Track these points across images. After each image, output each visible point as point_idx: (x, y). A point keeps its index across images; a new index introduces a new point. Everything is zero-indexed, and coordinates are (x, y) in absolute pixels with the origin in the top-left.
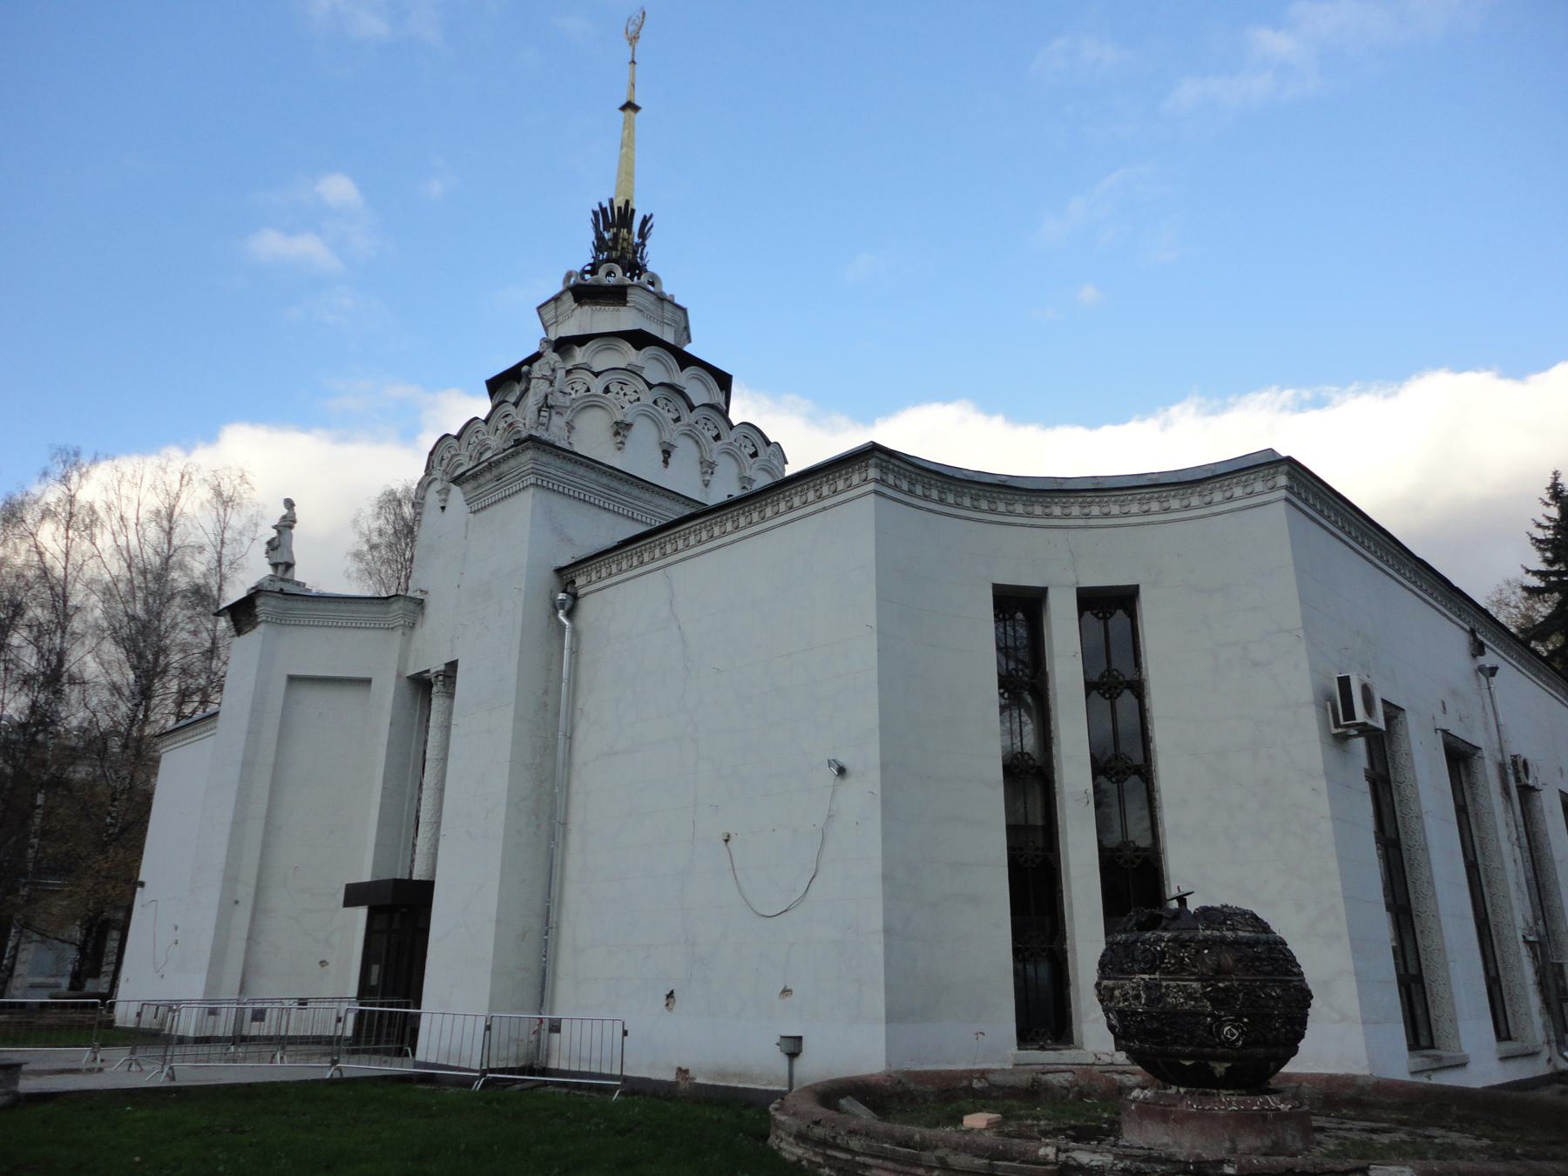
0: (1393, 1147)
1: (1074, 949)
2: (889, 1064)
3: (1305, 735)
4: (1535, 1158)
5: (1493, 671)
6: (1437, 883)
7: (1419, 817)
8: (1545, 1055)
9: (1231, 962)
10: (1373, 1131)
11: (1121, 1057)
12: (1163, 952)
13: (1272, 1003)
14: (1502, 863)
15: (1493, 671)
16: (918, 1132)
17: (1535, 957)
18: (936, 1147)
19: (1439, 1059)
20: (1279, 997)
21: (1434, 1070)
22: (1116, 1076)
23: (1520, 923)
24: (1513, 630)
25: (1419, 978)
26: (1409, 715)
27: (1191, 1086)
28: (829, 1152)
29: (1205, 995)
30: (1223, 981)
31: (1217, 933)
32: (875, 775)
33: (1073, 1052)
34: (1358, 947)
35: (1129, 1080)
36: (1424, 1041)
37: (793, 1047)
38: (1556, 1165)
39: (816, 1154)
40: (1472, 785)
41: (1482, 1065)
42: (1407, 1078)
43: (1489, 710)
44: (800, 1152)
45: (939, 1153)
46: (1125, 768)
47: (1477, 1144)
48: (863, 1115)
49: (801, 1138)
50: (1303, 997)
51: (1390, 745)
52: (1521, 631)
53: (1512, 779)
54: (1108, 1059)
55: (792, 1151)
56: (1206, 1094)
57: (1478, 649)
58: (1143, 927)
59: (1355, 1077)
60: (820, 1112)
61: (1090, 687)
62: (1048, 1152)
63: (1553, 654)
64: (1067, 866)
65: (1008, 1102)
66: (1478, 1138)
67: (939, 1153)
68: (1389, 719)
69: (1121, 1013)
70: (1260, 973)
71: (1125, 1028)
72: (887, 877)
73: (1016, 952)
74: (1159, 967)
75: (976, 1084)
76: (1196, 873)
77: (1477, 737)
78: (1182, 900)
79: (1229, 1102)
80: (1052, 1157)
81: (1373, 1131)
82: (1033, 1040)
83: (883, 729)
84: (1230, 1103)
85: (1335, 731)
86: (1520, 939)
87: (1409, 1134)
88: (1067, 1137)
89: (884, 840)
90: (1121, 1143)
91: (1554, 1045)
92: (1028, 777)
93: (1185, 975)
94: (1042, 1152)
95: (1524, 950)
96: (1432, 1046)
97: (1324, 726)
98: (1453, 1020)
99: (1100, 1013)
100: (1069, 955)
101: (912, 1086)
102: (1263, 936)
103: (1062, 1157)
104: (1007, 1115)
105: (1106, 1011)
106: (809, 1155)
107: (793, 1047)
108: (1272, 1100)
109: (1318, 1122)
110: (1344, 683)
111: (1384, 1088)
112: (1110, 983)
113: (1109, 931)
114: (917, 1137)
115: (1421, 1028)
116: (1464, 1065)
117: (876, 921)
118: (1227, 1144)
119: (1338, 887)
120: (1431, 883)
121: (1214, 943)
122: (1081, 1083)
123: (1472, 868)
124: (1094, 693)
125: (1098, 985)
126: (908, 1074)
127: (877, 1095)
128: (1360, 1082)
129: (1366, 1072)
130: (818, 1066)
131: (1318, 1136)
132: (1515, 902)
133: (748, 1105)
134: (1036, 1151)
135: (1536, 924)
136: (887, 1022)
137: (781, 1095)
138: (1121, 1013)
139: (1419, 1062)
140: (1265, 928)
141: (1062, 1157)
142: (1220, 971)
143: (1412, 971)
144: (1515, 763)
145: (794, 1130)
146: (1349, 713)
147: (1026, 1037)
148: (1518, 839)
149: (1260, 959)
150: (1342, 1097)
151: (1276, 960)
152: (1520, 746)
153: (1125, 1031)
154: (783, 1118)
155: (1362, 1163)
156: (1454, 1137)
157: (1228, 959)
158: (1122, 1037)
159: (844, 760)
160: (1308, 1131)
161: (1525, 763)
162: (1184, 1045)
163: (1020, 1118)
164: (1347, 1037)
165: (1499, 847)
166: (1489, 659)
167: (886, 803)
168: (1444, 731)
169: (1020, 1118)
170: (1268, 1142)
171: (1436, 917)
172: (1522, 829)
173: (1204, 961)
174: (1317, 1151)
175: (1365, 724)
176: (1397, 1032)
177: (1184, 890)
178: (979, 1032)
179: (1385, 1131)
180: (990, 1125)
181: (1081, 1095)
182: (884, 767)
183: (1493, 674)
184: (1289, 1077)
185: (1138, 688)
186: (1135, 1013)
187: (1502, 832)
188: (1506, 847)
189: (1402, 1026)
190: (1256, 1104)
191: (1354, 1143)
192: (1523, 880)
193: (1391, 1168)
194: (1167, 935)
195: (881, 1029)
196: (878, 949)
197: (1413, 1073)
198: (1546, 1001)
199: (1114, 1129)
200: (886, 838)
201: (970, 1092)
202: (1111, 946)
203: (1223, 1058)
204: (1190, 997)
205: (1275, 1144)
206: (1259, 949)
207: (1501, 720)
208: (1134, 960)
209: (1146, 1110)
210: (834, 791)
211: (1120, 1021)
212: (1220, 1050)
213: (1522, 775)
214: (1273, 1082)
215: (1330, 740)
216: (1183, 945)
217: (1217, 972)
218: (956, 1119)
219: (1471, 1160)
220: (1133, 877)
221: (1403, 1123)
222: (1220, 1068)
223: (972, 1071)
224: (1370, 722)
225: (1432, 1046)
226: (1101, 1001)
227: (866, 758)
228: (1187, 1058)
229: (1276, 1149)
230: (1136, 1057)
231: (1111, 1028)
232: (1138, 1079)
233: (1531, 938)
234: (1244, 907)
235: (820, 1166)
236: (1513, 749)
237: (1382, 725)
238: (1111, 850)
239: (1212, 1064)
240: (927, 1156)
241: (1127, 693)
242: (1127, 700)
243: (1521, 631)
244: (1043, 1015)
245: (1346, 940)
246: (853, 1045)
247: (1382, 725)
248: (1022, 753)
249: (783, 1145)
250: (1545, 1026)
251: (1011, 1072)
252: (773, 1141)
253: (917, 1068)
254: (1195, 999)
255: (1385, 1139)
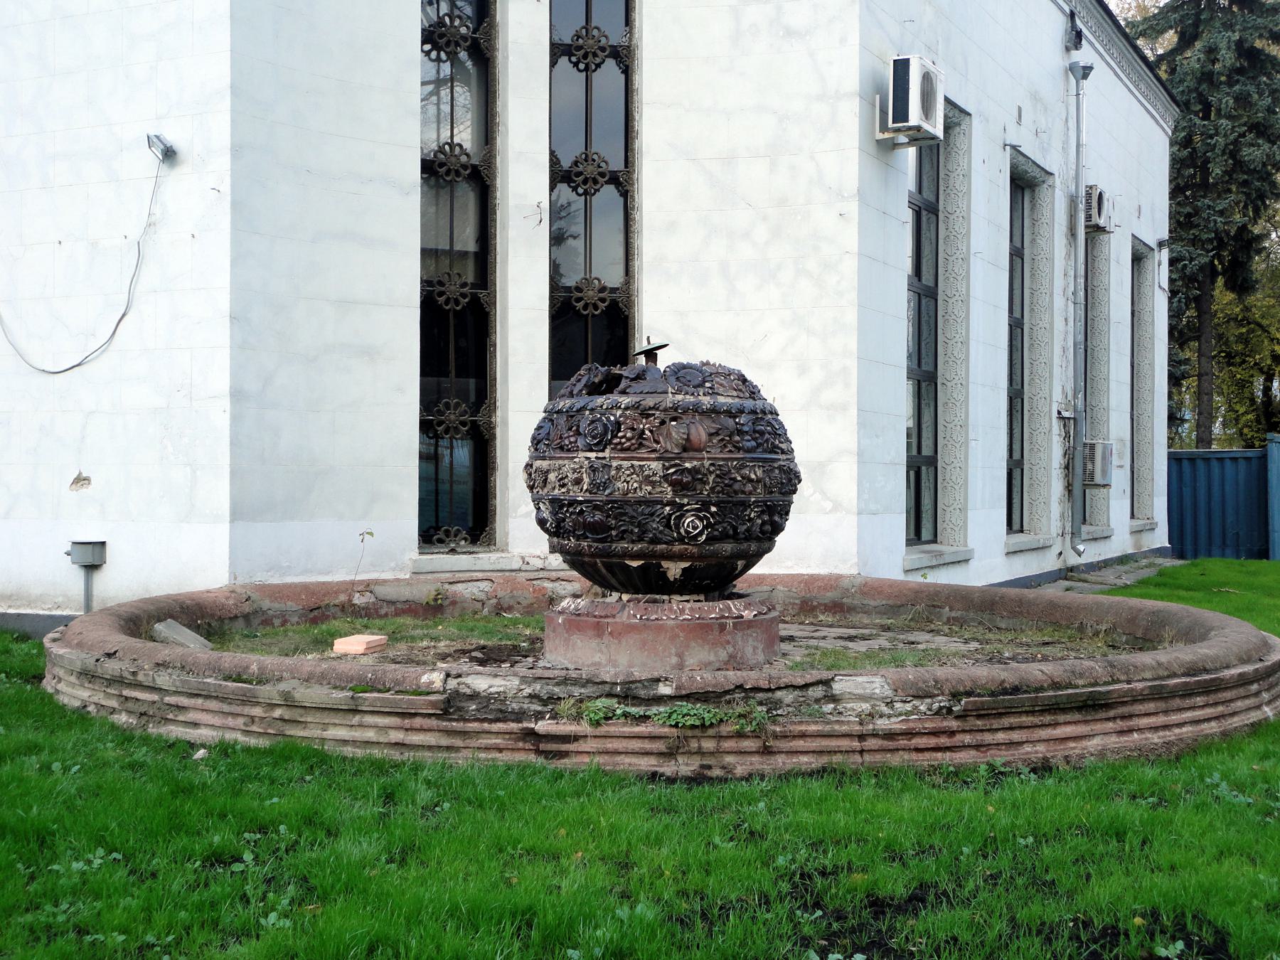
0: (869, 655)
1: (505, 423)
3: (848, 125)
5: (1086, 71)
7: (966, 260)
8: (1056, 550)
9: (704, 437)
10: (851, 638)
11: (556, 561)
12: (618, 424)
13: (749, 487)
15: (1086, 71)
16: (255, 661)
18: (280, 679)
19: (941, 554)
20: (759, 481)
21: (932, 567)
22: (547, 585)
23: (1057, 396)
24: (1123, 23)
25: (933, 461)
28: (126, 692)
29: (665, 477)
31: (690, 399)
32: (223, 163)
33: (494, 556)
36: (926, 534)
37: (91, 557)
39: (108, 695)
40: (1034, 222)
41: (985, 556)
42: (898, 575)
44: (85, 694)
45: (283, 686)
46: (596, 176)
47: (963, 647)
48: (191, 644)
49: (88, 676)
52: (1128, 23)
53: (1082, 217)
54: (538, 564)
55: (72, 693)
56: (655, 601)
57: (1076, 39)
58: (594, 390)
59: (839, 577)
60: (119, 641)
61: (558, 51)
62: (434, 678)
63: (1160, 58)
64: (505, 309)
65: (400, 620)
67: (283, 686)
68: (947, 128)
69: (556, 503)
70: (739, 449)
71: (559, 522)
74: (610, 442)
75: (358, 600)
76: (675, 321)
78: (651, 354)
79: (681, 608)
80: (438, 685)
81: (851, 638)
82: (440, 541)
83: (236, 90)
84: (682, 611)
85: (880, 136)
86: (1055, 414)
87: (890, 640)
88: (472, 659)
90: (541, 663)
91: (1068, 537)
92: (459, 178)
93: (643, 453)
95: (1056, 427)
96: (934, 541)
97: (866, 131)
98: (964, 510)
99: (531, 507)
100: (498, 431)
101: (266, 604)
102: (749, 404)
103: (452, 684)
104: (394, 637)
105: (537, 501)
106: (99, 698)
107: (91, 557)
108: (735, 606)
109: (785, 630)
110: (901, 67)
111: (871, 588)
112: (544, 464)
113: (552, 395)
114: (254, 667)
115: (923, 521)
116: (967, 561)
117: (218, 378)
118: (674, 660)
119: (853, 345)
121: (685, 411)
122: (500, 594)
123: (1016, 326)
124: (563, 61)
125: (529, 466)
127: (207, 618)
129: (854, 571)
130: (124, 581)
131: (785, 647)
132: (1057, 371)
133: (24, 638)
135: (1075, 397)
136: (232, 521)
137: (66, 621)
138: (556, 503)
139: (919, 556)
140: (754, 393)
141: (452, 684)
142: (688, 447)
143: (927, 451)
144: (1089, 195)
145: (78, 666)
146: (901, 112)
149: (740, 432)
150: (826, 602)
151: (762, 433)
152: (1096, 176)
153: (560, 523)
154: (61, 651)
155: (826, 675)
156: (940, 640)
157: (700, 432)
159: (173, 137)
160: (774, 640)
162: (633, 542)
163: (413, 639)
164: (833, 531)
166: (1084, 55)
169: (413, 639)
170: (723, 655)
175: (918, 128)
176: (898, 524)
177: (655, 342)
178: (371, 531)
179: (864, 638)
180: (370, 649)
181: (499, 609)
182: (237, 151)
183: (1085, 76)
184: (761, 579)
185: (624, 58)
187: (1059, 282)
194: (625, 401)
195: (223, 531)
196: (220, 416)
197: (907, 571)
198: (1069, 488)
199: (535, 647)
200: (237, 260)
201: (349, 610)
203: (680, 557)
204: (647, 480)
208: (578, 433)
209: (576, 622)
210: (157, 185)
211: (554, 513)
212: (677, 548)
213: (1094, 211)
214: (740, 585)
215: (872, 148)
216: (645, 414)
217: (685, 449)
218: (324, 643)
219: (954, 665)
220: (594, 330)
222: (674, 570)
223: (353, 583)
224: (926, 126)
226: (531, 488)
227: (208, 135)
228: (635, 556)
230: (575, 560)
231: (541, 523)
235: (113, 711)
236: (1089, 178)
237: (939, 131)
239: (665, 564)
241: (610, 64)
242: (609, 72)
243: (1128, 23)
244: (456, 509)
245: (854, 412)
246: (182, 548)
247: (939, 131)
249: (61, 686)
250: (1062, 516)
251: (408, 582)
252: (48, 685)
254: (653, 484)
255: (861, 646)
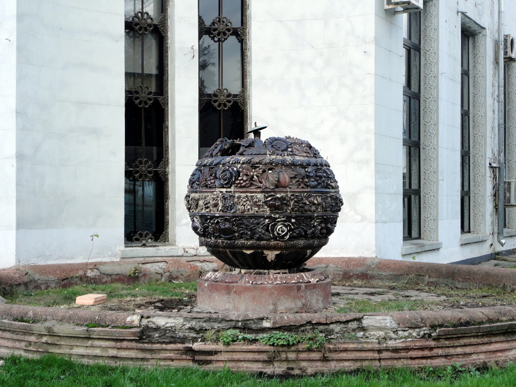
0: (383, 304)
1: (174, 172)
6: (441, 126)
8: (489, 243)
9: (288, 179)
10: (372, 294)
11: (204, 250)
12: (238, 172)
13: (313, 208)
14: (485, 113)
17: (495, 177)
18: (45, 320)
20: (319, 204)
22: (198, 264)
25: (418, 192)
29: (266, 203)
31: (279, 158)
33: (168, 248)
36: (414, 234)
38: (483, 310)
41: (449, 246)
45: (47, 324)
47: (437, 299)
50: (337, 204)
51: (425, 20)
53: (502, 53)
54: (193, 252)
56: (260, 273)
58: (225, 153)
59: (365, 259)
64: (173, 107)
65: (114, 285)
66: (438, 296)
67: (47, 324)
70: (308, 186)
71: (205, 229)
72: (20, 113)
75: (90, 274)
76: (274, 112)
77: (484, 20)
78: (257, 133)
79: (275, 278)
80: (136, 323)
81: (372, 294)
82: (137, 240)
84: (276, 279)
85: (387, 7)
87: (395, 295)
88: (156, 307)
90: (195, 310)
93: (253, 188)
94: (129, 319)
95: (489, 172)
96: (419, 238)
98: (436, 220)
100: (170, 177)
101: (37, 277)
102: (313, 160)
104: (111, 295)
105: (192, 217)
108: (306, 276)
109: (334, 289)
112: (196, 195)
113: (201, 156)
114: (31, 313)
115: (413, 225)
118: (271, 307)
119: (372, 125)
120: (436, 125)
122: (171, 269)
123: (465, 115)
125: (187, 196)
126: (35, 268)
128: (369, 262)
129: (374, 255)
131: (335, 299)
132: (489, 140)
135: (499, 155)
140: (316, 154)
141: (145, 322)
143: (414, 187)
144: (506, 40)
147: (131, 236)
149: (308, 177)
150: (358, 273)
151: (321, 177)
155: (358, 315)
157: (285, 176)
161: (512, 41)
163: (122, 296)
164: (364, 233)
165: (485, 101)
167: (19, 49)
168: (463, 13)
169: (122, 296)
170: (299, 304)
171: (436, 149)
177: (259, 125)
179: (380, 294)
180: (97, 302)
181: (171, 278)
182: (20, 17)
184: (321, 260)
186: (213, 217)
188: (489, 101)
189: (402, 224)
190: (294, 278)
192: (496, 124)
193: (378, 318)
194: (242, 159)
197: (403, 255)
200: (20, 78)
202: (200, 167)
203: (274, 248)
204: (256, 204)
205: (304, 305)
206: (309, 169)
207: (503, 8)
208: (215, 178)
209: (215, 286)
211: (202, 223)
212: (273, 243)
213: (509, 50)
214: (309, 264)
215: (383, 14)
216: (254, 166)
218: (70, 299)
220: (224, 119)
221: (393, 288)
222: (271, 255)
223: (87, 264)
226: (189, 209)
228: (248, 248)
229: (454, 343)
230: (214, 250)
231: (195, 229)
232: (211, 266)
233: (494, 165)
234: (303, 139)
236: (506, 31)
238: (209, 95)
239: (266, 252)
240: (38, 327)
244: (146, 221)
245: (372, 165)
248: (142, 13)
250: (492, 223)
251: (118, 263)
254: (259, 206)
255: (378, 299)
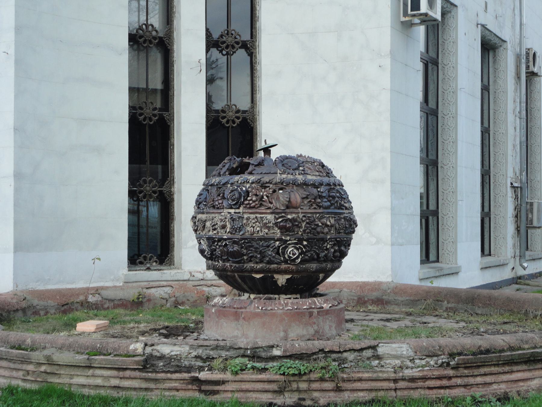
0: (399, 331)
1: (180, 191)
2: (16, 285)
4: (493, 333)
8: (510, 266)
9: (299, 200)
10: (388, 320)
11: (211, 274)
12: (247, 192)
13: (326, 230)
14: (507, 130)
17: (516, 198)
18: (45, 348)
19: (441, 269)
20: (332, 226)
21: (436, 277)
22: (206, 289)
26: (460, 10)
27: (259, 293)
29: (276, 224)
30: (291, 213)
31: (290, 177)
34: (396, 190)
35: (214, 291)
36: (432, 257)
41: (468, 270)
42: (417, 283)
43: (517, 12)
45: (46, 352)
47: (456, 326)
53: (524, 67)
54: (200, 276)
56: (270, 299)
58: (233, 172)
59: (380, 283)
64: (179, 123)
65: (117, 311)
67: (46, 352)
68: (443, 14)
69: (211, 240)
70: (320, 207)
71: (212, 251)
73: (132, 194)
75: (91, 299)
76: (281, 131)
77: (505, 33)
78: (267, 151)
79: (286, 303)
80: (140, 351)
81: (388, 320)
82: (141, 263)
84: (287, 305)
85: (403, 19)
86: (509, 185)
87: (412, 321)
88: (160, 334)
89: (16, 96)
90: (202, 337)
91: (518, 259)
93: (262, 209)
94: (132, 347)
95: (510, 192)
96: (437, 261)
97: (395, 15)
98: (455, 242)
100: (176, 197)
101: (35, 302)
102: (326, 180)
104: (113, 321)
105: (199, 239)
108: (318, 301)
109: (348, 315)
111: (400, 290)
112: (203, 217)
114: (29, 341)
116: (457, 273)
118: (282, 334)
120: (455, 142)
122: (177, 294)
123: (485, 132)
125: (194, 217)
128: (384, 287)
129: (389, 280)
131: (349, 325)
132: (510, 159)
134: (128, 347)
135: (521, 174)
138: (211, 240)
140: (329, 173)
141: (148, 350)
143: (432, 207)
144: (528, 54)
147: (135, 259)
148: (520, 112)
149: (321, 197)
150: (373, 299)
151: (334, 197)
152: (533, 43)
153: (213, 251)
155: (373, 343)
156: (442, 322)
157: (297, 197)
158: (210, 256)
160: (343, 322)
161: (534, 55)
163: (125, 322)
164: (377, 255)
168: (483, 26)
169: (125, 322)
170: (311, 331)
171: (455, 168)
172: (524, 105)
173: (278, 198)
174: (346, 336)
175: (426, 15)
176: (415, 251)
177: (269, 143)
180: (99, 329)
182: (18, 29)
184: (334, 284)
187: (510, 105)
188: (511, 117)
191: (372, 330)
192: (518, 142)
193: (394, 345)
194: (252, 178)
197: (421, 280)
199: (198, 326)
200: (19, 94)
201: (86, 305)
203: (285, 272)
204: (265, 226)
205: (317, 332)
206: (322, 189)
207: (524, 21)
209: (222, 311)
211: (210, 246)
212: (283, 266)
213: (531, 64)
214: (321, 289)
216: (264, 186)
218: (71, 325)
219: (450, 337)
220: (233, 136)
222: (281, 280)
223: (88, 289)
224: (431, 13)
225: (437, 261)
226: (196, 231)
228: (258, 272)
230: (222, 274)
232: (219, 290)
233: (516, 185)
236: (528, 44)
237: (438, 17)
238: (217, 111)
239: (276, 276)
240: (37, 356)
244: (150, 244)
245: (388, 184)
247: (438, 17)
248: (147, 25)
250: (514, 245)
251: (121, 288)
253: (41, 287)
254: (269, 228)
255: (394, 325)
